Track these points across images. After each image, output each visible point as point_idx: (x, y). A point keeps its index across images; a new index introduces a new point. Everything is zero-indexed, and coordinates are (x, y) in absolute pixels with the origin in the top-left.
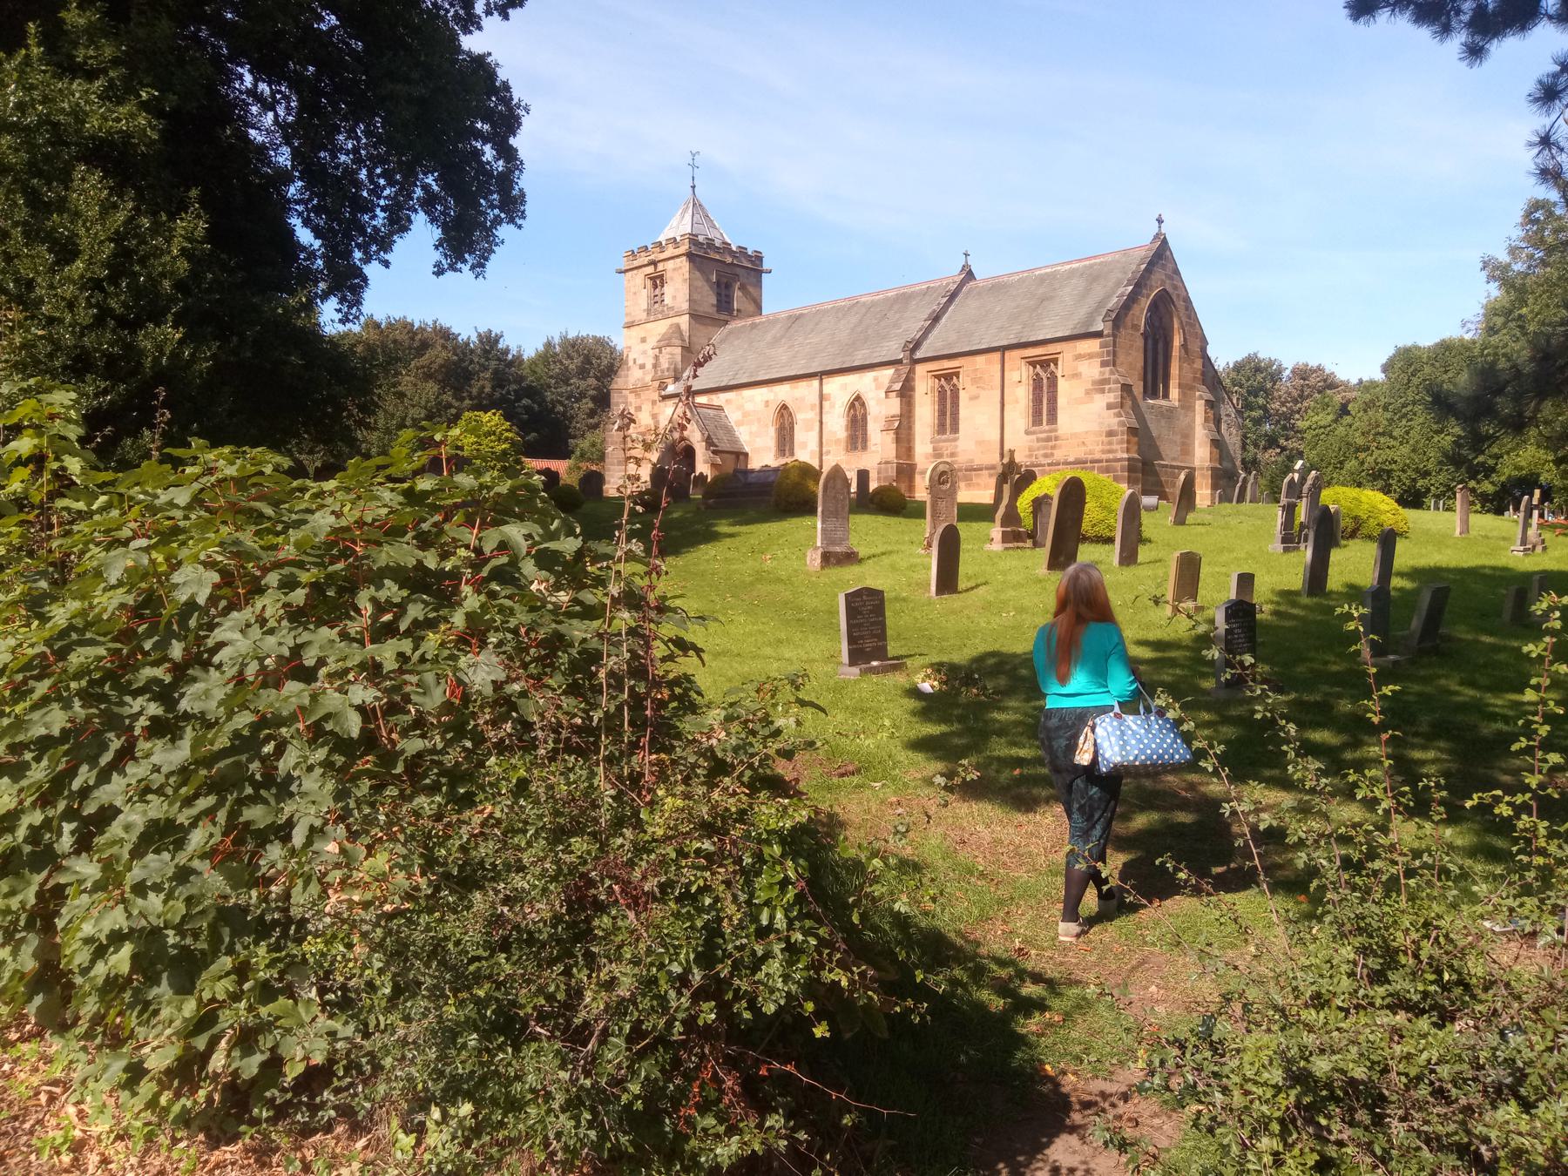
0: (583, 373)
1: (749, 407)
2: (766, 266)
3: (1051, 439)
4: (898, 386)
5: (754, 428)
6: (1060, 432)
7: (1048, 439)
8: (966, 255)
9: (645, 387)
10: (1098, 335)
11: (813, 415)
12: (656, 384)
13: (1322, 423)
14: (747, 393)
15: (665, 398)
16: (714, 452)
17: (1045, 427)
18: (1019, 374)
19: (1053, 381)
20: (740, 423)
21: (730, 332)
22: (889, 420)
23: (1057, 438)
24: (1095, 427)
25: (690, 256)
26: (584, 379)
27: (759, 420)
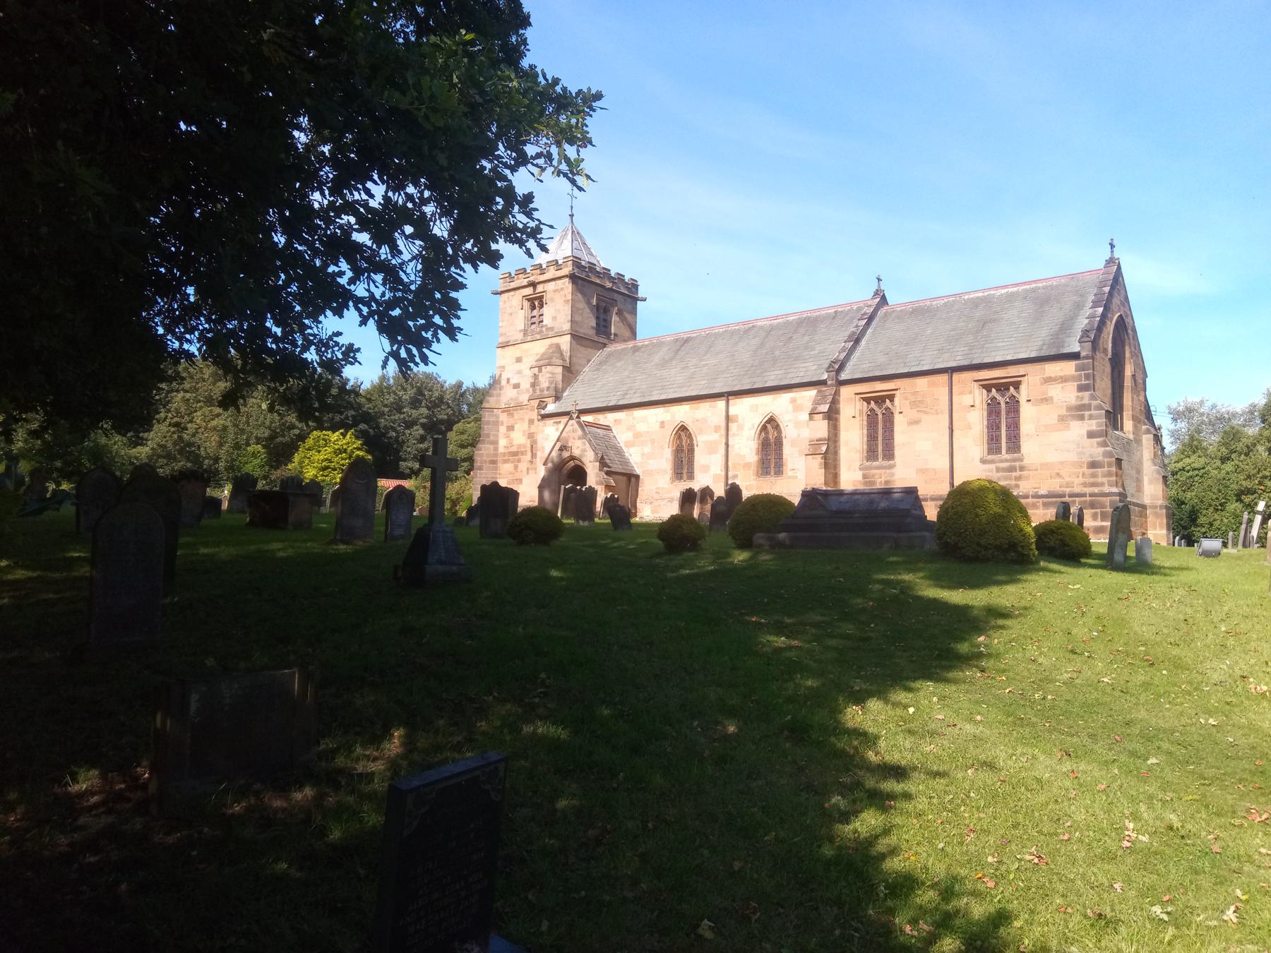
0: (415, 403)
1: (641, 427)
2: (641, 294)
3: (1016, 468)
4: (825, 408)
5: (647, 450)
6: (1026, 462)
7: (1012, 469)
8: (879, 280)
9: (519, 406)
10: (1074, 356)
11: (718, 437)
12: (535, 403)
13: (1196, 465)
14: (638, 413)
15: (544, 417)
16: (608, 473)
17: (1004, 455)
18: (971, 400)
19: (1014, 407)
20: (630, 444)
21: (610, 355)
22: (815, 444)
23: (1022, 468)
24: (1072, 457)
25: (572, 277)
26: (416, 408)
27: (653, 441)
